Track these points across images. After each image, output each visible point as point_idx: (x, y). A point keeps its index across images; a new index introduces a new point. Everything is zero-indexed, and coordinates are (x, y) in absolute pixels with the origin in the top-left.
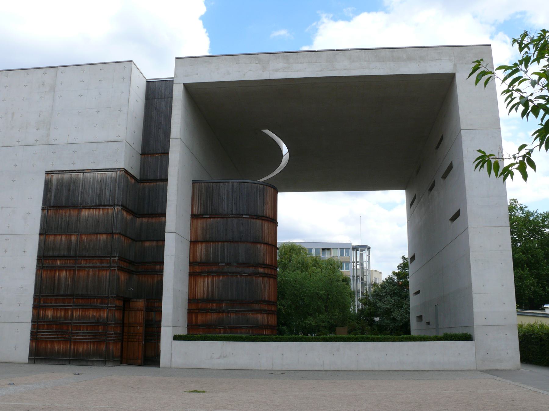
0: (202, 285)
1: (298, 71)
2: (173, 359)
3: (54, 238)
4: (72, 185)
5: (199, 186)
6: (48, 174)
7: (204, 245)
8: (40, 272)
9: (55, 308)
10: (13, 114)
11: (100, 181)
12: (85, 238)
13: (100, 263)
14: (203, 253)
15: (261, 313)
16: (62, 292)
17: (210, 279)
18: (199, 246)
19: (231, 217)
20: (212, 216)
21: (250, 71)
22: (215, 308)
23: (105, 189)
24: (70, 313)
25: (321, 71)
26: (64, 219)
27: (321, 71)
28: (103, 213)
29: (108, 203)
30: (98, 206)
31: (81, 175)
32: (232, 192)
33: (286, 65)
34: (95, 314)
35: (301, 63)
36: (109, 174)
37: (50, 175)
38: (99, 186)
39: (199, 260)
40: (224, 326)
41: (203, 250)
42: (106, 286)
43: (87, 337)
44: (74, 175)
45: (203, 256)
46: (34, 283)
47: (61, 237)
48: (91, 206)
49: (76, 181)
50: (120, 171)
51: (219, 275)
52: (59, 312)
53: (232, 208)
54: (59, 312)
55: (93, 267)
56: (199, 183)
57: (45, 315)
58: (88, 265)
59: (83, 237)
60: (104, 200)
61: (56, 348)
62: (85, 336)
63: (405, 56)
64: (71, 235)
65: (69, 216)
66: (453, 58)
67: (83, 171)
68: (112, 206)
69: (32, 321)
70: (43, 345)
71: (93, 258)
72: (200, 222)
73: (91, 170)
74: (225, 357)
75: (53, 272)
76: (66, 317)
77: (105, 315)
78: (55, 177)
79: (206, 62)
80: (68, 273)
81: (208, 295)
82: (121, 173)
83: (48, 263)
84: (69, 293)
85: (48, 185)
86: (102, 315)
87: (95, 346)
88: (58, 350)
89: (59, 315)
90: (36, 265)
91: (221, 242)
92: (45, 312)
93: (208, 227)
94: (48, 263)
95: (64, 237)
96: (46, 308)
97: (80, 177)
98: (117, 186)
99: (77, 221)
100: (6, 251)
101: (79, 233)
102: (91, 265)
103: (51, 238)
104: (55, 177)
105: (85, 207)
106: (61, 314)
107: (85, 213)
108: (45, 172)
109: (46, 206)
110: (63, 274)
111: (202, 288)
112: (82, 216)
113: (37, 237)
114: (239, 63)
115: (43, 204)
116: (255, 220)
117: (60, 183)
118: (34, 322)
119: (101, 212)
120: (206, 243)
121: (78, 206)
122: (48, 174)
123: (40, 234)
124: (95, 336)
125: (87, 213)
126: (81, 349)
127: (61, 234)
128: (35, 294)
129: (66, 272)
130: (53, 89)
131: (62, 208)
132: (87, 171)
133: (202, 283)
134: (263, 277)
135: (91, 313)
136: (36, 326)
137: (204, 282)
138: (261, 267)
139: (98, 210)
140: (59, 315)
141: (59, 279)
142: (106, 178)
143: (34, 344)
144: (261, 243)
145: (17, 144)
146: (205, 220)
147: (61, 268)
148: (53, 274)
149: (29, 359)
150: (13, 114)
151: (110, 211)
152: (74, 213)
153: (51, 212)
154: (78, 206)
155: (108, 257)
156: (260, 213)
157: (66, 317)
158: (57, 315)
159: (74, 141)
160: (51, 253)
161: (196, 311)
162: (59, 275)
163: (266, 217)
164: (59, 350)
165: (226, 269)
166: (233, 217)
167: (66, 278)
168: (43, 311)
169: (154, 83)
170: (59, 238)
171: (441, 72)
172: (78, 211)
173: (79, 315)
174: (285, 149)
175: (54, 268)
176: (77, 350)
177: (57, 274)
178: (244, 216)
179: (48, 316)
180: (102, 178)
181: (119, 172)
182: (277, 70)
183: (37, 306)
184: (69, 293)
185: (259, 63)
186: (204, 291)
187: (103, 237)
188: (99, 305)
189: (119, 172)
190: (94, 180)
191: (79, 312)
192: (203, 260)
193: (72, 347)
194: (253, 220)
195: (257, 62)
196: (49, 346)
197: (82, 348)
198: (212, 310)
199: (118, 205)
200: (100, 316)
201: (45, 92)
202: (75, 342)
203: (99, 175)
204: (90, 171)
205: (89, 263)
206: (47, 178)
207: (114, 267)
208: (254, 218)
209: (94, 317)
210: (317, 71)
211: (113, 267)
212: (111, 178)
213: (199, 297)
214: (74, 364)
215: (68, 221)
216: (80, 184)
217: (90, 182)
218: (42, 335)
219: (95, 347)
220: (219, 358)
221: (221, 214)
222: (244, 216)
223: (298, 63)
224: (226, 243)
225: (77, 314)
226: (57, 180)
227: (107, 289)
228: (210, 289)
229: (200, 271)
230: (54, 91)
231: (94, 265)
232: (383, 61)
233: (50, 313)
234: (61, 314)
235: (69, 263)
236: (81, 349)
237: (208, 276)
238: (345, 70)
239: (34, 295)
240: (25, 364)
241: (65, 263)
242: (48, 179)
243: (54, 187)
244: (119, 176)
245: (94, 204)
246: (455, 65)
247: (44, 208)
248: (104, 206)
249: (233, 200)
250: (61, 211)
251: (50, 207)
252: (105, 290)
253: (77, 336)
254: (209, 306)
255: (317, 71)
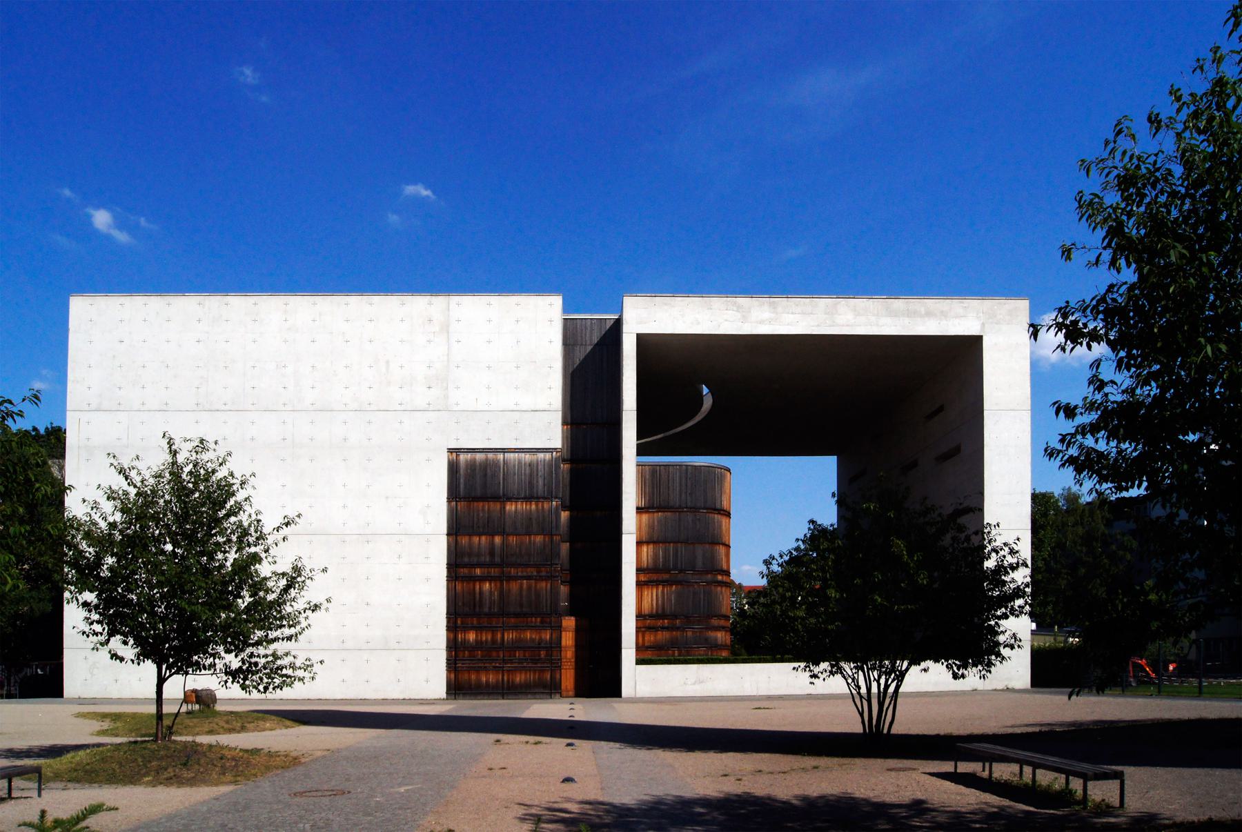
0: (650, 596)
1: (788, 325)
2: (638, 687)
3: (470, 540)
4: (489, 471)
5: (642, 470)
6: (451, 452)
7: (651, 546)
8: (453, 584)
9: (478, 629)
10: (388, 362)
11: (530, 465)
12: (513, 540)
13: (537, 572)
14: (649, 558)
15: (720, 630)
16: (486, 610)
17: (660, 588)
18: (645, 548)
19: (685, 511)
20: (661, 508)
21: (726, 320)
22: (666, 625)
23: (537, 475)
24: (499, 636)
25: (818, 326)
26: (481, 515)
27: (818, 326)
28: (537, 509)
29: (542, 495)
30: (528, 499)
31: (501, 456)
32: (687, 478)
33: (773, 315)
34: (534, 637)
35: (792, 313)
36: (541, 456)
37: (454, 454)
38: (528, 472)
39: (645, 565)
40: (678, 648)
41: (651, 553)
42: (546, 601)
43: (525, 665)
44: (490, 456)
45: (649, 561)
46: (445, 599)
47: (480, 539)
48: (520, 498)
49: (496, 464)
50: (557, 452)
51: (671, 585)
52: (484, 635)
53: (687, 500)
54: (484, 635)
55: (528, 578)
56: (642, 466)
57: (465, 641)
58: (520, 574)
59: (511, 538)
60: (537, 491)
61: (484, 679)
62: (522, 663)
63: (923, 310)
64: (493, 535)
65: (489, 509)
66: (982, 315)
67: (504, 451)
68: (548, 498)
69: (447, 647)
70: (466, 676)
71: (527, 566)
72: (645, 517)
73: (515, 449)
74: (702, 682)
75: (472, 584)
76: (494, 641)
77: (548, 637)
78: (463, 457)
79: (666, 304)
80: (493, 585)
81: (663, 608)
82: (558, 454)
83: (464, 571)
84: (496, 610)
85: (453, 469)
86: (543, 637)
87: (537, 674)
88: (486, 682)
89: (484, 638)
90: (446, 575)
91: (674, 542)
92: (465, 636)
93: (656, 523)
94: (464, 571)
95: (483, 538)
96: (466, 629)
97: (500, 459)
98: (554, 472)
99: (501, 518)
100: (399, 557)
101: (503, 533)
102: (525, 574)
103: (464, 540)
104: (463, 457)
105: (510, 499)
106: (486, 637)
107: (510, 507)
108: (447, 450)
109: (454, 494)
110: (487, 586)
111: (650, 600)
112: (507, 512)
113: (444, 538)
114: (711, 309)
115: (448, 493)
116: (713, 515)
117: (472, 465)
118: (450, 648)
119: (533, 507)
120: (648, 545)
121: (500, 498)
122: (451, 452)
123: (448, 534)
124: (536, 664)
125: (513, 507)
126: (518, 679)
127: (480, 535)
128: (448, 613)
129: (490, 584)
130: (446, 328)
131: (484, 498)
132: (509, 450)
133: (650, 594)
134: (722, 586)
135: (528, 635)
136: (453, 653)
137: (652, 594)
138: (720, 574)
139: (528, 503)
140: (484, 638)
141: (481, 593)
142: (538, 464)
143: (453, 676)
144: (720, 544)
145: (399, 408)
146: (651, 514)
147: (482, 579)
148: (472, 587)
149: (447, 693)
150: (388, 362)
151: (546, 506)
152: (496, 506)
153: (462, 505)
154: (500, 498)
155: (549, 565)
156: (718, 507)
157: (494, 641)
158: (481, 638)
159: (486, 408)
160: (466, 560)
161: (643, 629)
162: (480, 588)
163: (724, 510)
164: (487, 681)
165: (680, 577)
166: (687, 512)
167: (491, 592)
168: (461, 634)
169: (575, 321)
170: (476, 539)
171: (966, 334)
172: (501, 505)
173: (512, 638)
174: (708, 402)
175: (472, 579)
176: (512, 681)
177: (478, 587)
178: (701, 511)
179: (469, 640)
180: (531, 461)
181: (554, 453)
182: (761, 322)
183: (452, 627)
184: (496, 610)
185: (738, 311)
186: (652, 605)
187: (539, 539)
188: (538, 624)
189: (554, 453)
190: (520, 462)
191: (512, 633)
192: (651, 566)
193: (505, 678)
194: (710, 515)
195: (735, 309)
196: (473, 677)
197: (519, 678)
198: (663, 628)
199: (556, 498)
200: (540, 638)
201: (434, 332)
202: (508, 671)
203: (527, 457)
204: (514, 450)
205: (522, 572)
206: (450, 457)
207: (557, 577)
208: (711, 513)
209: (532, 640)
210: (813, 326)
211: (554, 577)
212: (545, 460)
213: (647, 612)
214: (510, 697)
215: (488, 518)
216: (500, 467)
217: (514, 466)
218: (463, 664)
219: (537, 677)
220: (694, 684)
221: (672, 508)
222: (701, 511)
223: (789, 313)
224: (679, 545)
225: (510, 636)
226: (467, 461)
227: (549, 605)
228: (660, 602)
229: (646, 579)
230: (448, 333)
231: (530, 574)
232: (896, 316)
233: (472, 636)
234: (486, 637)
235: (494, 572)
236: (518, 679)
237: (657, 585)
238: (848, 326)
239: (447, 614)
240: (444, 699)
241: (488, 572)
242: (453, 460)
243: (462, 472)
244: (556, 458)
245: (523, 496)
246: (983, 324)
247: (449, 500)
248: (538, 498)
249: (687, 489)
250: (475, 504)
251: (460, 499)
252: (546, 606)
253: (512, 663)
254: (660, 623)
255: (813, 326)
